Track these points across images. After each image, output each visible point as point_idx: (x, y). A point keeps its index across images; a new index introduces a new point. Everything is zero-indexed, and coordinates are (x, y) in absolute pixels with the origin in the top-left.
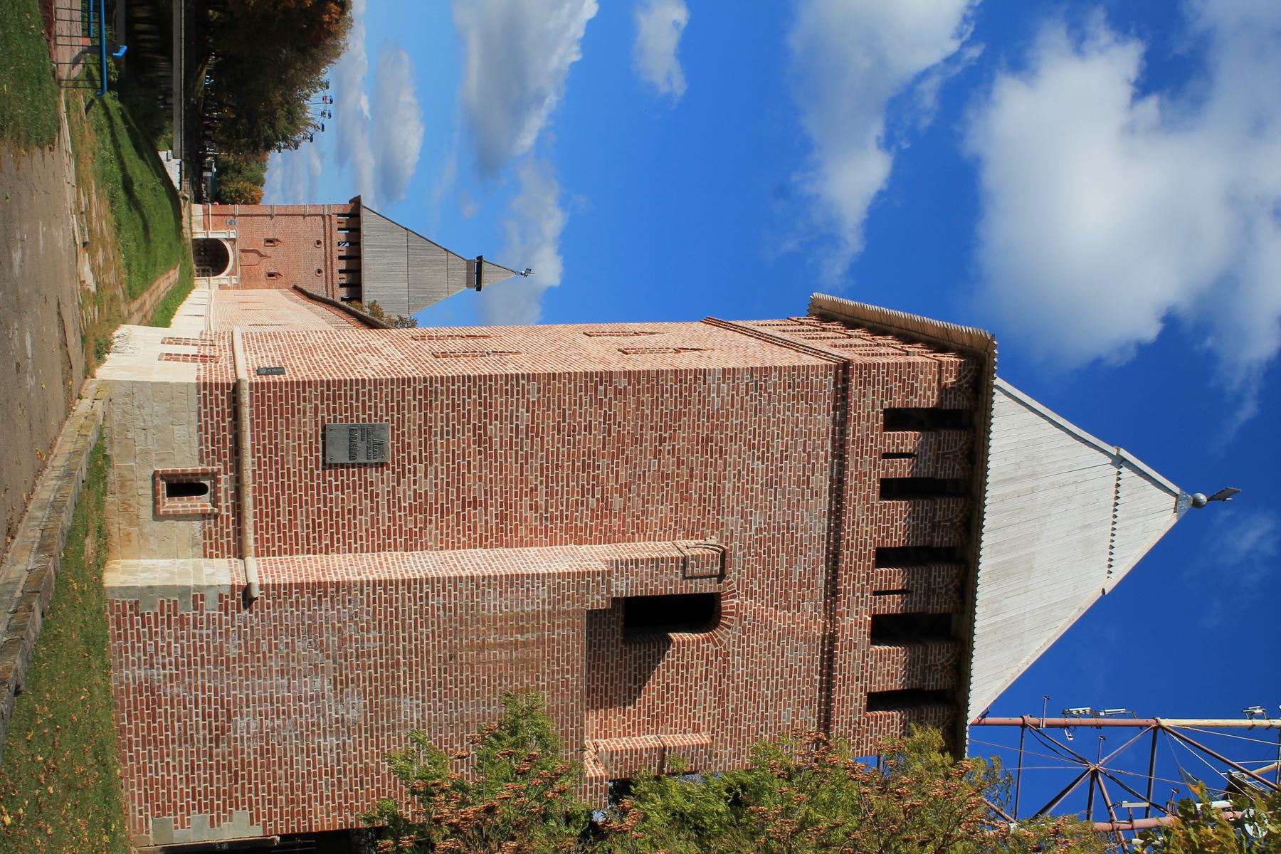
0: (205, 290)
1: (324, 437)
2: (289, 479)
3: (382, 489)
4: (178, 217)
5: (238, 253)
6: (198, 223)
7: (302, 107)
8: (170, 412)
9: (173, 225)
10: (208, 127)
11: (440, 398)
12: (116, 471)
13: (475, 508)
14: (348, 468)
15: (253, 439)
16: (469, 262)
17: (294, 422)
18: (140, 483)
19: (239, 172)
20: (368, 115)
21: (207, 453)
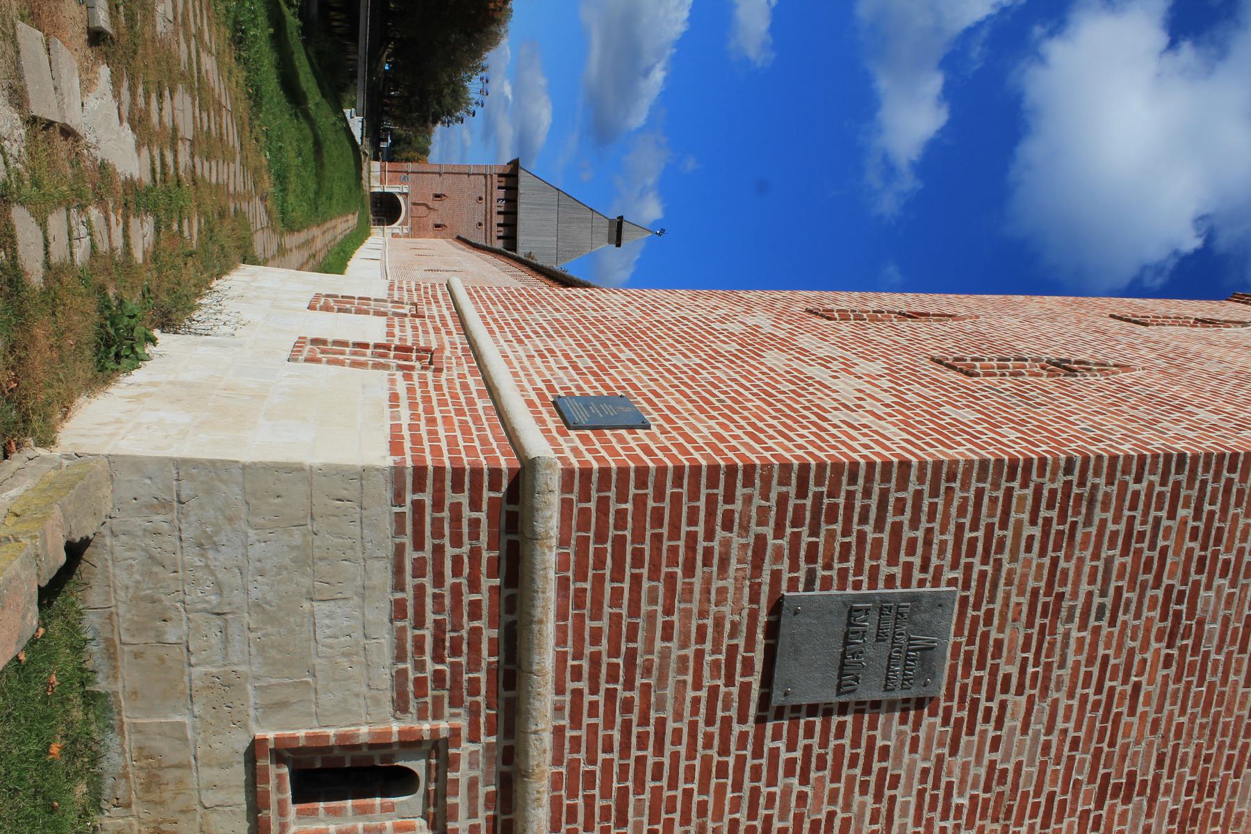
0: (379, 237)
1: (772, 631)
2: (659, 750)
3: (910, 764)
4: (359, 168)
5: (410, 206)
6: (375, 178)
7: (464, 88)
8: (305, 560)
9: (353, 170)
10: (386, 105)
11: (1098, 515)
12: (130, 741)
13: (1127, 800)
14: (828, 713)
15: (561, 641)
16: (611, 221)
17: (689, 590)
18: (208, 774)
19: (410, 143)
20: (513, 95)
21: (420, 683)
